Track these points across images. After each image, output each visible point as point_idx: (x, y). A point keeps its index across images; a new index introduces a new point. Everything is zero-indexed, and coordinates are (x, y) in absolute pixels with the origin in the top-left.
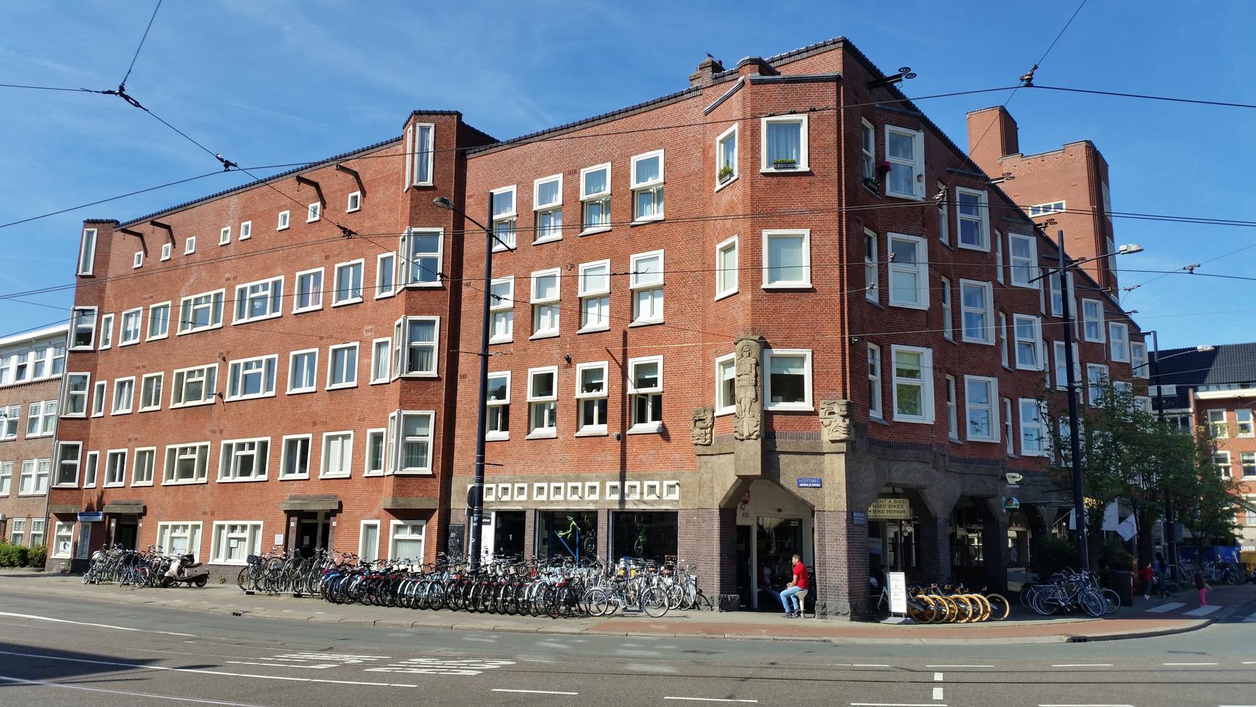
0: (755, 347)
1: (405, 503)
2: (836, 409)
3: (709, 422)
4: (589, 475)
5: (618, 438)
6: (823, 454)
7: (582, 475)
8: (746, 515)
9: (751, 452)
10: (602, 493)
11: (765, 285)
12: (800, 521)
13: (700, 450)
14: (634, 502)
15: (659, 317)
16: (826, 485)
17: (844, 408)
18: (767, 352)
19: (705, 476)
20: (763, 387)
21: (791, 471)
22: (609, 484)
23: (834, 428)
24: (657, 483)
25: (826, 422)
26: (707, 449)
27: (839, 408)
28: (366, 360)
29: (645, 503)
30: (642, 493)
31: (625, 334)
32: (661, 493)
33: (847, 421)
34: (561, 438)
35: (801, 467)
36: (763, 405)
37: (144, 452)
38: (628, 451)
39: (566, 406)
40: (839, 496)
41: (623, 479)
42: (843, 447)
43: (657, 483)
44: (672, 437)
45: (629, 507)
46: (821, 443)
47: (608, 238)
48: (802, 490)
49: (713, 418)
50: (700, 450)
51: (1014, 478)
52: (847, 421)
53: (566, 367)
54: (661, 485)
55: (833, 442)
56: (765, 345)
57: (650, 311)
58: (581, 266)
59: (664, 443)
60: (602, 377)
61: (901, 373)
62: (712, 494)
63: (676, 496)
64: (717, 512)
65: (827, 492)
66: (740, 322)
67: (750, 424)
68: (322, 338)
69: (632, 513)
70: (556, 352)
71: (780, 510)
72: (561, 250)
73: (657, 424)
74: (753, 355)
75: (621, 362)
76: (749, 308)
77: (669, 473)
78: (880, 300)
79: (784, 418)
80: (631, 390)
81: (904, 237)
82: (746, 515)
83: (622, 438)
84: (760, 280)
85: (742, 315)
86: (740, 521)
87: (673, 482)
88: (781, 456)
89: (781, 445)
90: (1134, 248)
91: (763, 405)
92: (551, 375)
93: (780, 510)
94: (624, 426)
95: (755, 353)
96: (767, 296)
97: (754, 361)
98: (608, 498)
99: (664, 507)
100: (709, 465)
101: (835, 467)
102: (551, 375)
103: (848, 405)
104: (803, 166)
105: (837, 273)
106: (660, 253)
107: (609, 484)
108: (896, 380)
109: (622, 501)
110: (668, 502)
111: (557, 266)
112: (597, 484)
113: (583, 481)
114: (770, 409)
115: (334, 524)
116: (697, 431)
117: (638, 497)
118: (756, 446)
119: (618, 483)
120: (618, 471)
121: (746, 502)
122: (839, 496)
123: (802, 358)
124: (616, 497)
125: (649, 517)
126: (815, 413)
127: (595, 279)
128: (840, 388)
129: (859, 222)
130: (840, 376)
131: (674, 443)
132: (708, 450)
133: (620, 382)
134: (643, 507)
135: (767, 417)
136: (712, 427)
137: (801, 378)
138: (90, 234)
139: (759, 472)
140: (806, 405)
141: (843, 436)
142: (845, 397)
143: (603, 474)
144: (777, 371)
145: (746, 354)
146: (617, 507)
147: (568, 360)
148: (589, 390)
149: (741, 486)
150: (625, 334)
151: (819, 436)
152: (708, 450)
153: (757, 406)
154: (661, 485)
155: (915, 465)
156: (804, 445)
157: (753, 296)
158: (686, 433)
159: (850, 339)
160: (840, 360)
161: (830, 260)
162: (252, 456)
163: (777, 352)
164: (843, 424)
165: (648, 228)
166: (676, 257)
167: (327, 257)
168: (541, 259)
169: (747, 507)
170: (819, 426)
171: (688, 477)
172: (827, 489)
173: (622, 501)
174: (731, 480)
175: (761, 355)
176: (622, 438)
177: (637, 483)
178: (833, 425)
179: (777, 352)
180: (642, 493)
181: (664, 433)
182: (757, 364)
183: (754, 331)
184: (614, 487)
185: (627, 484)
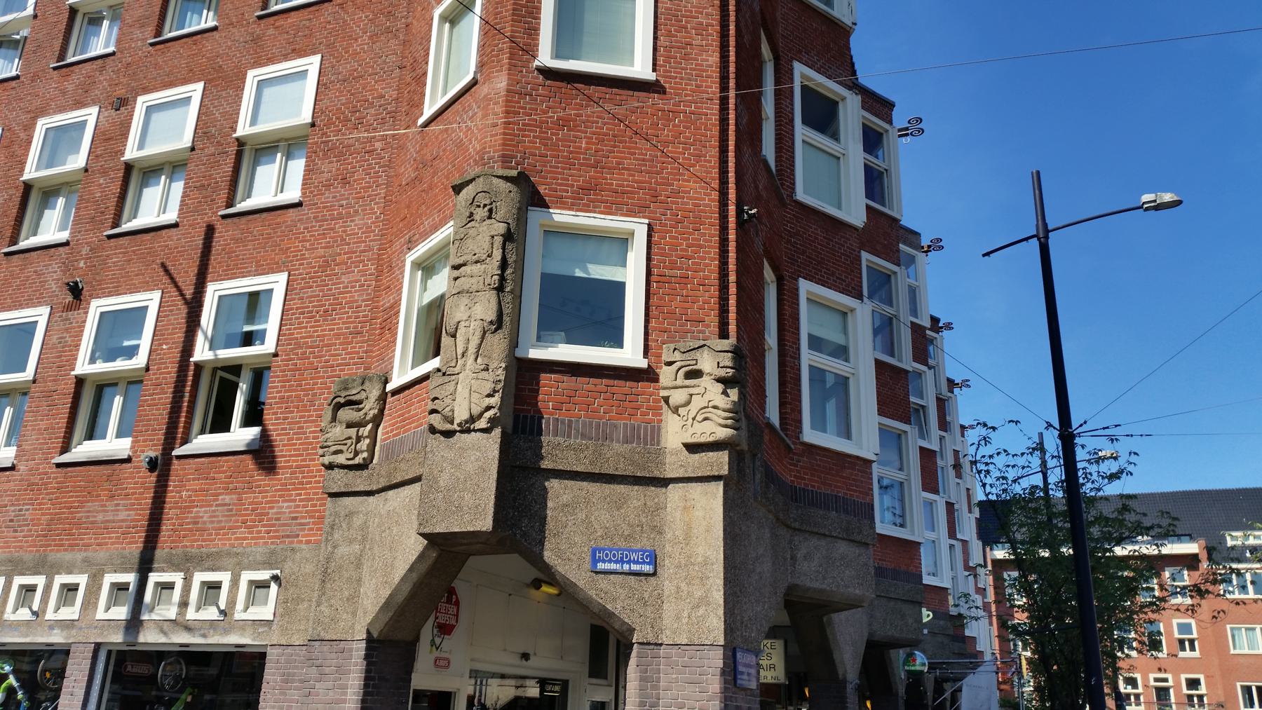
0: (507, 196)
2: (707, 363)
3: (370, 407)
4: (67, 556)
5: (152, 464)
6: (664, 482)
7: (54, 556)
8: (442, 664)
9: (470, 468)
10: (90, 602)
11: (545, 57)
12: (565, 684)
13: (340, 480)
14: (163, 625)
15: (293, 193)
16: (668, 568)
17: (727, 360)
18: (535, 215)
19: (343, 550)
20: (518, 297)
21: (577, 527)
22: (109, 579)
23: (697, 412)
24: (224, 577)
25: (677, 397)
26: (358, 477)
27: (714, 360)
29: (188, 628)
30: (184, 604)
31: (210, 230)
32: (232, 602)
33: (734, 394)
35: (602, 517)
36: (514, 344)
38: (171, 497)
39: (49, 394)
40: (704, 601)
41: (145, 566)
42: (720, 462)
43: (224, 577)
44: (281, 462)
45: (149, 637)
46: (660, 452)
47: (208, 44)
48: (603, 582)
49: (383, 398)
50: (340, 480)
51: (925, 631)
52: (734, 394)
53: (69, 308)
54: (235, 582)
55: (692, 448)
56: (533, 199)
57: (273, 184)
59: (259, 477)
60: (138, 334)
61: (817, 343)
62: (353, 599)
63: (265, 611)
64: (359, 649)
65: (668, 587)
66: (474, 147)
67: (473, 390)
69: (156, 656)
70: (53, 275)
71: (525, 656)
72: (109, 73)
73: (254, 431)
74: (500, 215)
75: (189, 292)
76: (499, 109)
77: (259, 551)
79: (568, 382)
80: (201, 353)
81: (820, 79)
82: (442, 664)
83: (161, 467)
84: (530, 50)
85: (481, 132)
86: (424, 678)
87: (264, 575)
88: (553, 485)
89: (557, 449)
90: (1168, 197)
91: (514, 344)
93: (525, 656)
94: (174, 434)
95: (505, 210)
96: (544, 88)
97: (501, 228)
98: (101, 614)
99: (234, 639)
100: (358, 521)
101: (696, 519)
103: (737, 353)
105: (714, 59)
106: (312, 64)
107: (109, 579)
108: (808, 358)
109: (134, 623)
110: (244, 625)
111: (94, 103)
112: (82, 580)
113: (50, 570)
114: (535, 354)
116: (338, 431)
117: (172, 613)
118: (484, 451)
119: (130, 578)
120: (135, 549)
121: (445, 630)
122: (704, 601)
123: (623, 241)
124: (121, 613)
126: (647, 375)
127: (167, 122)
128: (713, 320)
130: (714, 291)
131: (283, 475)
132: (360, 481)
133: (180, 336)
134: (182, 638)
135: (524, 377)
136: (377, 420)
137: (619, 288)
139: (485, 523)
140: (630, 354)
141: (723, 433)
142: (724, 335)
143: (101, 555)
144: (557, 268)
145: (480, 213)
146: (117, 638)
147: (76, 291)
148: (110, 357)
149: (432, 572)
150: (210, 230)
151: (654, 434)
152: (360, 481)
153: (498, 344)
154: (235, 582)
155: (842, 548)
156: (616, 456)
157: (512, 82)
158: (307, 433)
159: (740, 212)
160: (714, 252)
161: (700, 29)
163: (562, 216)
164: (721, 401)
165: (294, 17)
166: (344, 69)
168: (64, 93)
169: (448, 643)
170: (657, 410)
171: (303, 563)
172: (668, 581)
173: (134, 623)
174: (413, 546)
175: (522, 219)
176: (161, 467)
177: (177, 578)
178: (697, 403)
179: (562, 216)
180: (184, 604)
181: (262, 455)
182: (508, 237)
183: (506, 160)
184: (121, 588)
185: (154, 578)
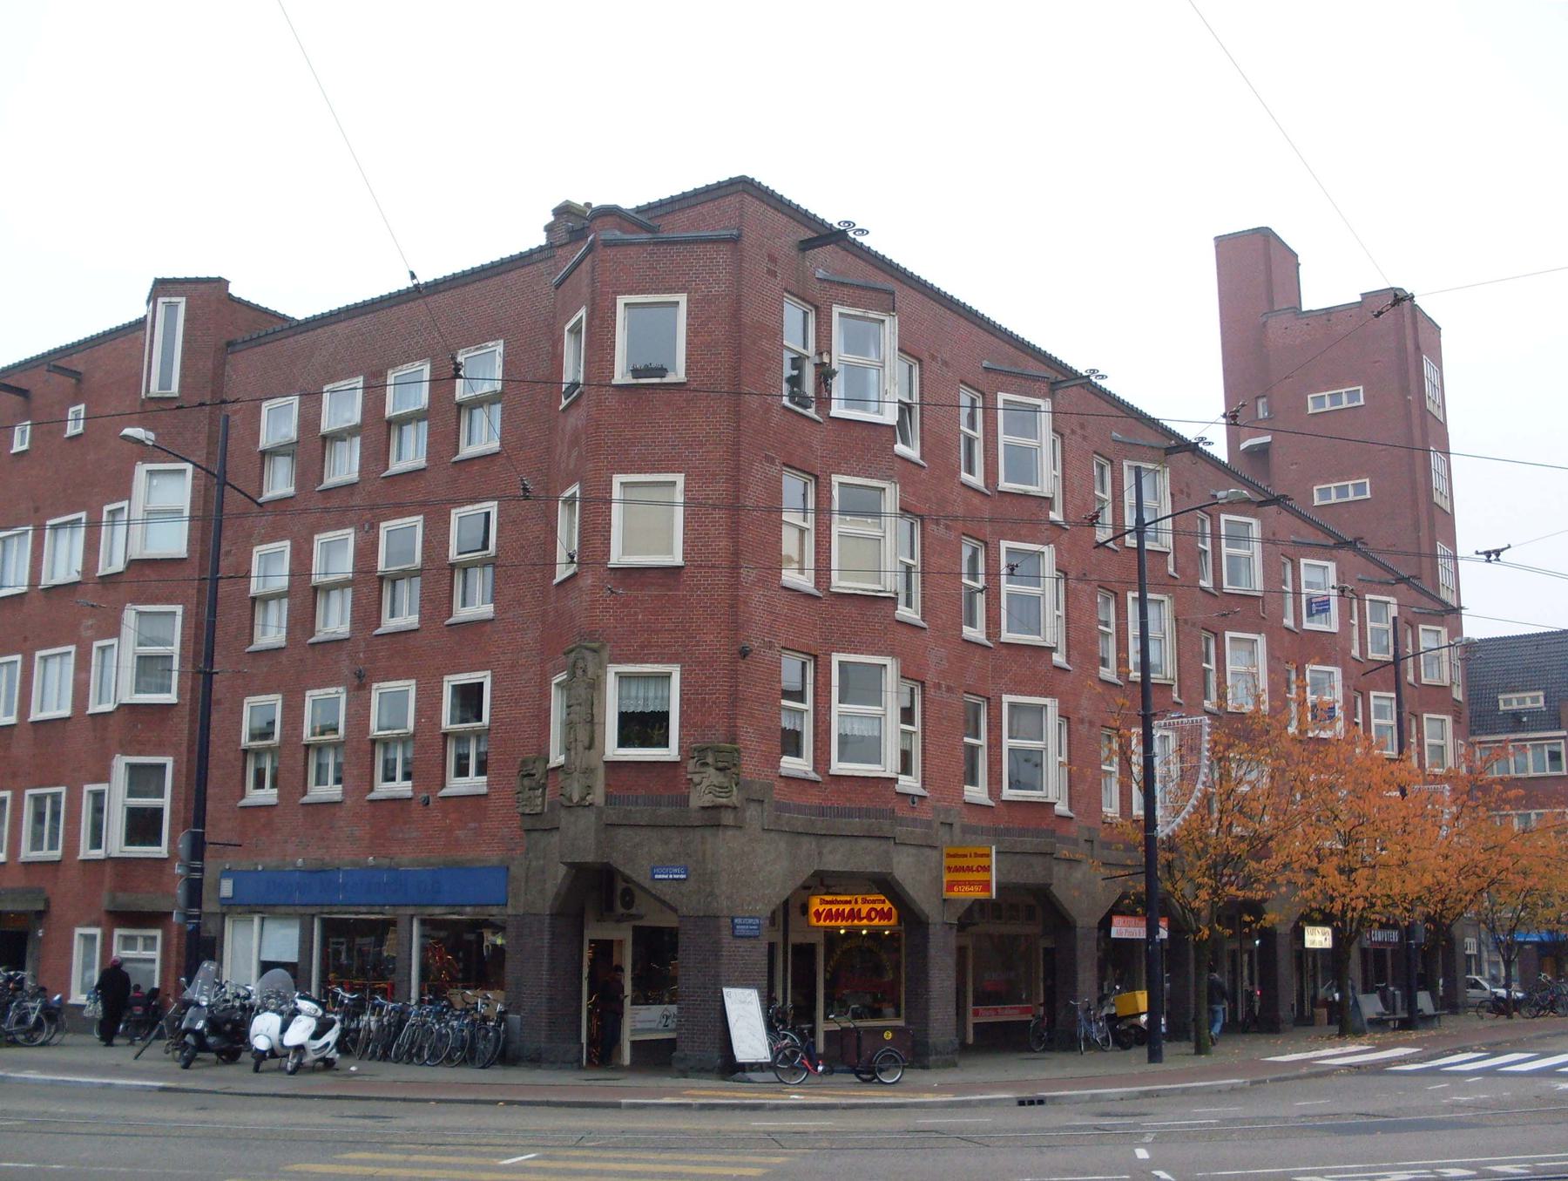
1: (127, 900)
25: (697, 778)
28: (83, 676)
34: (349, 802)
37: (44, 796)
48: (659, 886)
57: (475, 605)
58: (382, 525)
68: (25, 639)
70: (345, 667)
78: (817, 584)
92: (481, 684)
102: (481, 684)
104: (679, 374)
115: (40, 933)
125: (657, 931)
129: (771, 460)
136: (544, 787)
138: (171, 307)
151: (685, 801)
162: (158, 812)
167: (37, 510)
174: (558, 874)
178: (706, 783)
